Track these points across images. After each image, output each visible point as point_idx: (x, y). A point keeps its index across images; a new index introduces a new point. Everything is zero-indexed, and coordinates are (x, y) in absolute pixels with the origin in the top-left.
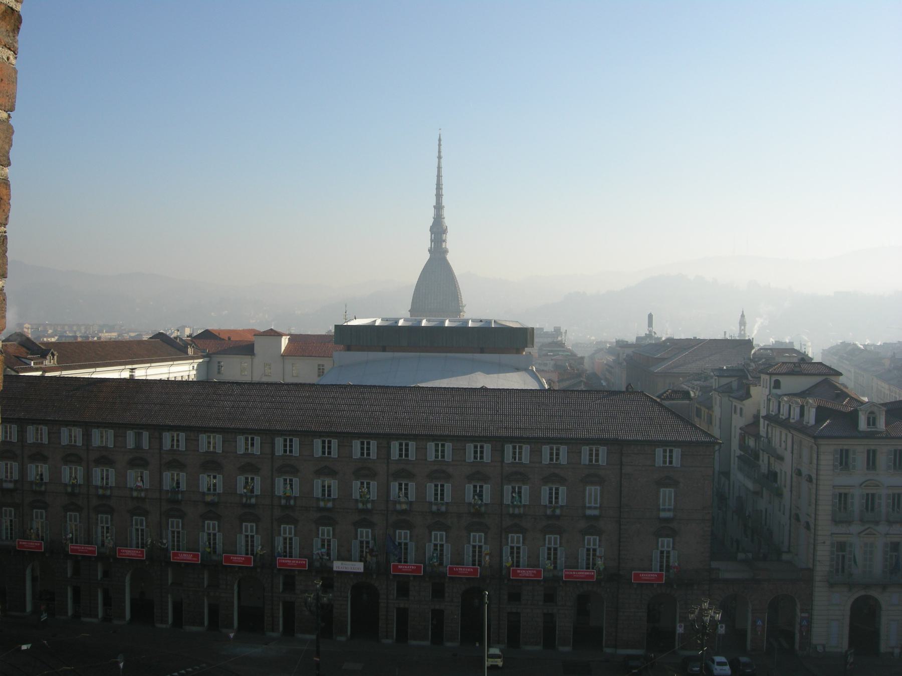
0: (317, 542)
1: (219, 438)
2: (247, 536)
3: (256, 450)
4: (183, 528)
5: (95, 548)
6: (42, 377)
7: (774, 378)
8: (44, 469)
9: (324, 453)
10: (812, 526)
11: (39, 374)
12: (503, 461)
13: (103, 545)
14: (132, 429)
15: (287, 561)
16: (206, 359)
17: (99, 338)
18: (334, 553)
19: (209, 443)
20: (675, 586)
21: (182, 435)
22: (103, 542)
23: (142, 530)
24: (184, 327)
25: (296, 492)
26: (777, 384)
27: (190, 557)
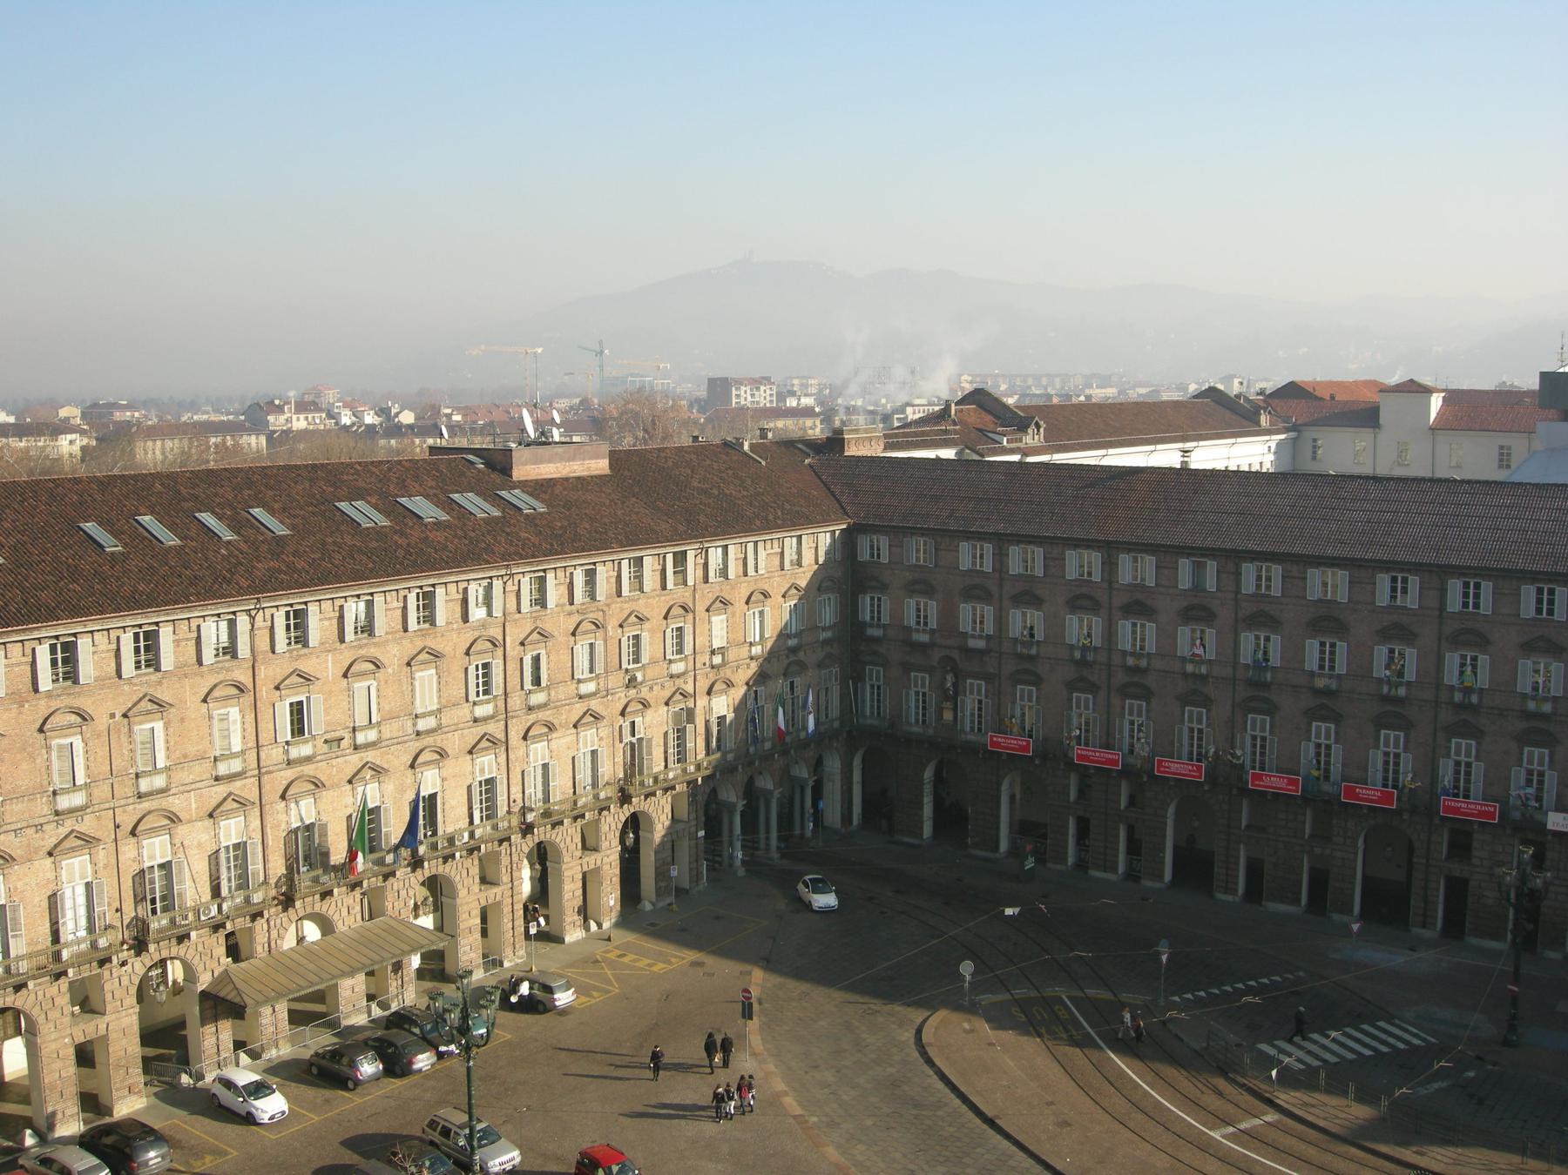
0: (1518, 775)
1: (1342, 576)
2: (1318, 746)
3: (1411, 600)
4: (1271, 733)
5: (1118, 756)
6: (1020, 463)
8: (1035, 617)
9: (1539, 611)
11: (1015, 458)
13: (1131, 751)
14: (1188, 555)
15: (1460, 804)
16: (1293, 434)
17: (1088, 397)
18: (1549, 796)
19: (1325, 584)
20: (1509, 831)
21: (1277, 570)
22: (1132, 745)
23: (1200, 731)
24: (1232, 377)
25: (1483, 681)
27: (1282, 784)
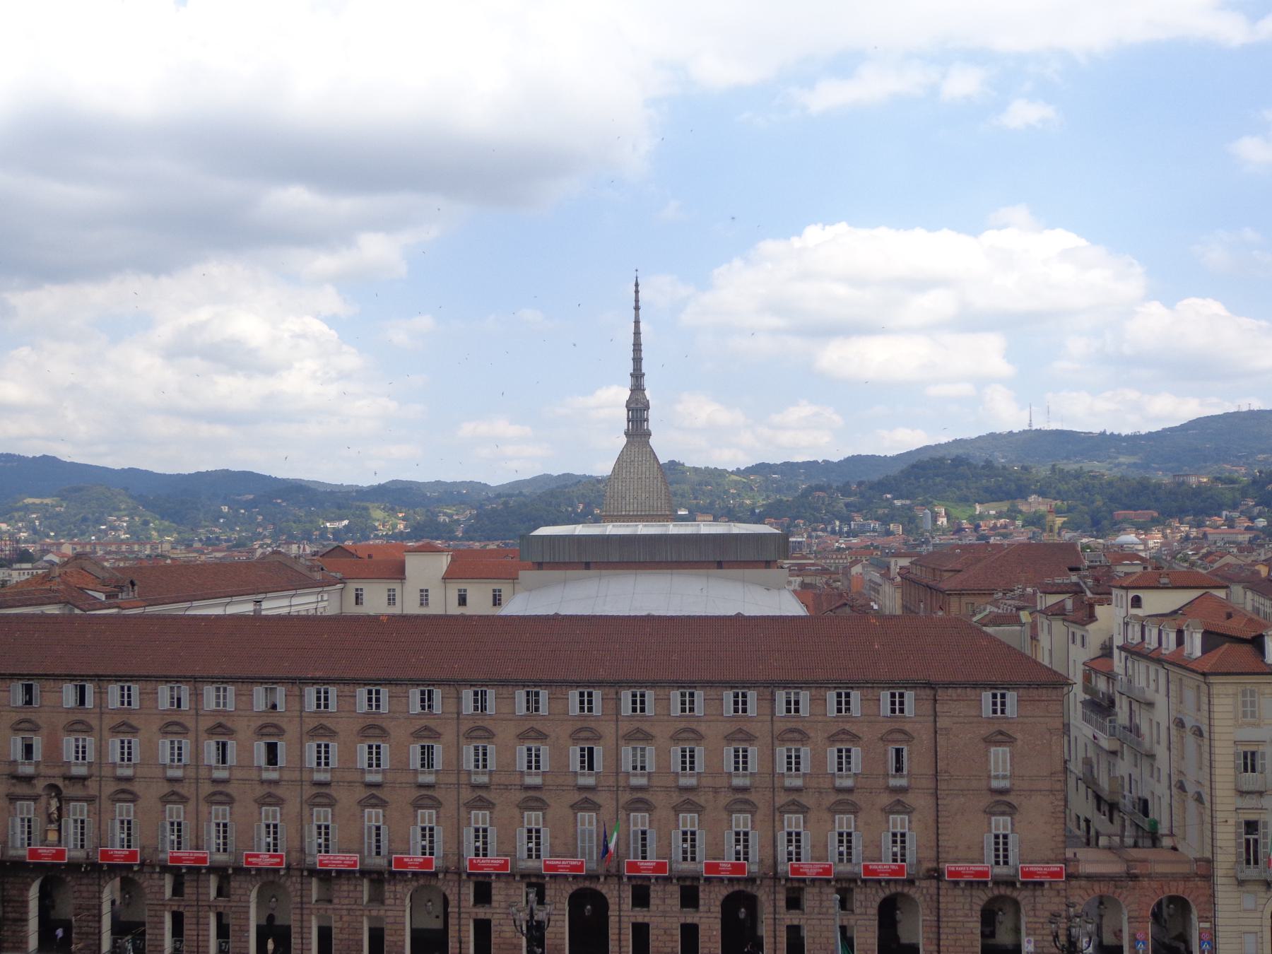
7: (1132, 593)
10: (1206, 798)
12: (773, 714)
26: (1137, 602)
